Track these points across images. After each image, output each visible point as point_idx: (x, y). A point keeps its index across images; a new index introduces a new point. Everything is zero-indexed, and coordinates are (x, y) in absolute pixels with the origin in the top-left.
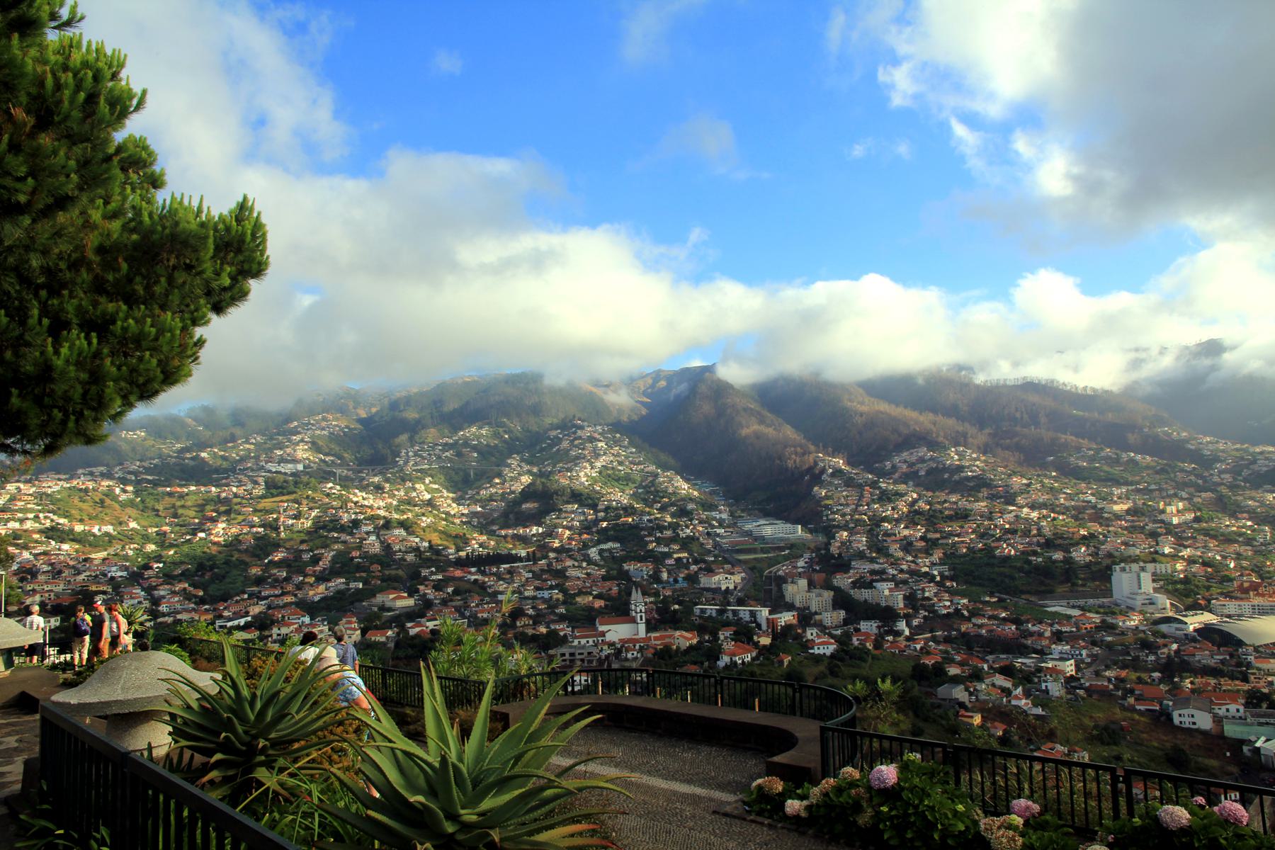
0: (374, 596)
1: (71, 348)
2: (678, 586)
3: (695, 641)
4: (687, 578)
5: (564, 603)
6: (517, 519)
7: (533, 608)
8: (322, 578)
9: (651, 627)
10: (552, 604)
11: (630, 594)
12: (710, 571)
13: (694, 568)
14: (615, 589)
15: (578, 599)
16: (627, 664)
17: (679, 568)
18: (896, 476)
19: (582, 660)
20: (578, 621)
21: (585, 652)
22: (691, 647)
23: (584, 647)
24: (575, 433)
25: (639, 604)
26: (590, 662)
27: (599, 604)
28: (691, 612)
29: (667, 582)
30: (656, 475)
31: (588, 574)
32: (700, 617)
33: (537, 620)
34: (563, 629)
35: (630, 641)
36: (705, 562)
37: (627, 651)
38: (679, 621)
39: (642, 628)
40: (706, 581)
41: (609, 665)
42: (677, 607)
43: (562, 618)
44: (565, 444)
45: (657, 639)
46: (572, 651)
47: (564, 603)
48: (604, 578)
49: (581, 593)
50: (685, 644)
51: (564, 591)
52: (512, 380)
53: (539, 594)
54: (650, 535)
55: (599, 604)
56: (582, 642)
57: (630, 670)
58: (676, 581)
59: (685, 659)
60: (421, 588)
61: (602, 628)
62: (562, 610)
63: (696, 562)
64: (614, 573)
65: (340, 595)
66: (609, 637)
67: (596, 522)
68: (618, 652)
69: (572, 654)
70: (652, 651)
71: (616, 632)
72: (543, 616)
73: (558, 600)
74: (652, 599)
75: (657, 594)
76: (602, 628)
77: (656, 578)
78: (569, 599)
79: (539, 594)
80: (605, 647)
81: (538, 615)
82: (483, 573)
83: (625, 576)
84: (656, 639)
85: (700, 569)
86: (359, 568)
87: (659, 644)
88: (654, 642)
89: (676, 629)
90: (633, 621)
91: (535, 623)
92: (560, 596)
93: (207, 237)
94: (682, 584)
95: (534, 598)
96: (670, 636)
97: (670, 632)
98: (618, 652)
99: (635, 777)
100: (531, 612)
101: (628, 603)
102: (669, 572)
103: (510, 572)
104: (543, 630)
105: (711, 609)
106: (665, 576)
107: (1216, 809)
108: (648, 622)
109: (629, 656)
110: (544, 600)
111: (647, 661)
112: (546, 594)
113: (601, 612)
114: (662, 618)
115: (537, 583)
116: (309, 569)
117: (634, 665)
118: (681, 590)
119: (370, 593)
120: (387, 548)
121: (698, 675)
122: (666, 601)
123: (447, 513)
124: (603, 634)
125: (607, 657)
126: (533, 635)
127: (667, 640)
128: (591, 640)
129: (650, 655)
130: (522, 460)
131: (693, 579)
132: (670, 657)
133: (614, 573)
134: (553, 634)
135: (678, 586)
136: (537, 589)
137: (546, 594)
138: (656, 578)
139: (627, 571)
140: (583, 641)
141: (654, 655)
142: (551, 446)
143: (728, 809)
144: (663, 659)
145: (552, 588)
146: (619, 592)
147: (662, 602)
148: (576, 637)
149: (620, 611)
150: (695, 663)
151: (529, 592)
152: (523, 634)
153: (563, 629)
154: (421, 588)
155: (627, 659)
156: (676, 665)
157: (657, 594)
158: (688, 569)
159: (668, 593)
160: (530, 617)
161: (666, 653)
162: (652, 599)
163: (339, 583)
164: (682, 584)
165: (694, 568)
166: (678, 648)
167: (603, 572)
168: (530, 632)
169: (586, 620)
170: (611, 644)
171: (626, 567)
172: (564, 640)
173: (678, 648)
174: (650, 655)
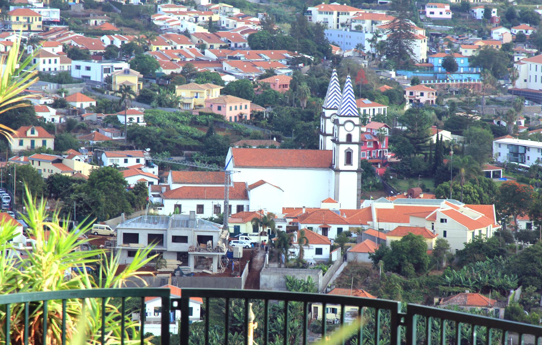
2: (454, 80)
3: (489, 231)
4: (485, 61)
5: (144, 98)
7: (58, 104)
9: (373, 182)
10: (110, 105)
11: (321, 91)
13: (502, 34)
14: (283, 74)
15: (183, 92)
16: (301, 276)
17: (461, 31)
18: (29, 260)
19: (183, 257)
20: (177, 150)
21: (192, 236)
22: (477, 248)
23: (188, 222)
25: (346, 121)
26: (202, 261)
27: (236, 109)
28: (482, 152)
29: (428, 67)
31: (213, 27)
32: (509, 168)
33: (67, 137)
34: (136, 168)
35: (311, 215)
37: (304, 241)
38: (449, 174)
39: (350, 182)
41: (254, 279)
42: (446, 135)
43: (135, 140)
45: (389, 217)
46: (156, 229)
47: (144, 98)
48: (257, 43)
49: (189, 76)
50: (460, 237)
51: (145, 67)
53: (77, 69)
55: (236, 109)
56: (183, 208)
57: (308, 299)
58: (450, 66)
59: (461, 274)
61: (240, 175)
62: (135, 117)
63: (509, 19)
64: (285, 29)
66: (257, 202)
68: (279, 244)
69: (156, 238)
70: (373, 247)
71: (281, 189)
72: (85, 129)
73: (126, 89)
74: (380, 109)
75: (394, 97)
76: (240, 175)
77: (395, 52)
78: (156, 89)
79: (77, 69)
80: (247, 227)
81: (70, 126)
83: (311, 42)
84: (384, 215)
85: (520, 39)
87: (391, 232)
88: (376, 224)
89: (439, 195)
90: (328, 163)
91: (59, 148)
92: (134, 80)
94: (465, 76)
95: (63, 78)
96: (422, 213)
97: (424, 202)
98: (279, 244)
99: (228, 193)
100: (51, 115)
101: (313, 116)
102: (433, 40)
104: (81, 166)
106: (420, 49)
107: (232, 185)
108: (366, 170)
109: (309, 255)
110: (91, 88)
111: (354, 275)
112: (96, 71)
113: (239, 132)
114: (410, 162)
115: (73, 38)
117: (321, 281)
118: (463, 90)
121: (490, 324)
122: (415, 117)
124: (243, 192)
125: (249, 254)
127: (414, 222)
128: (209, 205)
129: (364, 259)
132: (419, 267)
133: (285, 29)
134: (107, 179)
135: (454, 80)
136: (73, 54)
137: (96, 71)
138: (395, 52)
139: (320, 28)
140: (189, 206)
141: (376, 258)
143: (309, 316)
144: (398, 270)
145: (110, 54)
146: (294, 84)
147: (410, 118)
148: (170, 194)
149: (294, 131)
150: (486, 290)
151: (51, 62)
153: (136, 168)
155: (301, 264)
156: (434, 289)
158: (485, 35)
159: (427, 97)
160: (50, 128)
161: (404, 257)
162: (380, 109)
164: (465, 76)
165: (502, 34)
166: (442, 246)
167: (254, 24)
168: (46, 169)
169: (202, 147)
170: (262, 221)
171: (317, 16)
172: (135, 200)
173: (442, 246)
174: (364, 259)
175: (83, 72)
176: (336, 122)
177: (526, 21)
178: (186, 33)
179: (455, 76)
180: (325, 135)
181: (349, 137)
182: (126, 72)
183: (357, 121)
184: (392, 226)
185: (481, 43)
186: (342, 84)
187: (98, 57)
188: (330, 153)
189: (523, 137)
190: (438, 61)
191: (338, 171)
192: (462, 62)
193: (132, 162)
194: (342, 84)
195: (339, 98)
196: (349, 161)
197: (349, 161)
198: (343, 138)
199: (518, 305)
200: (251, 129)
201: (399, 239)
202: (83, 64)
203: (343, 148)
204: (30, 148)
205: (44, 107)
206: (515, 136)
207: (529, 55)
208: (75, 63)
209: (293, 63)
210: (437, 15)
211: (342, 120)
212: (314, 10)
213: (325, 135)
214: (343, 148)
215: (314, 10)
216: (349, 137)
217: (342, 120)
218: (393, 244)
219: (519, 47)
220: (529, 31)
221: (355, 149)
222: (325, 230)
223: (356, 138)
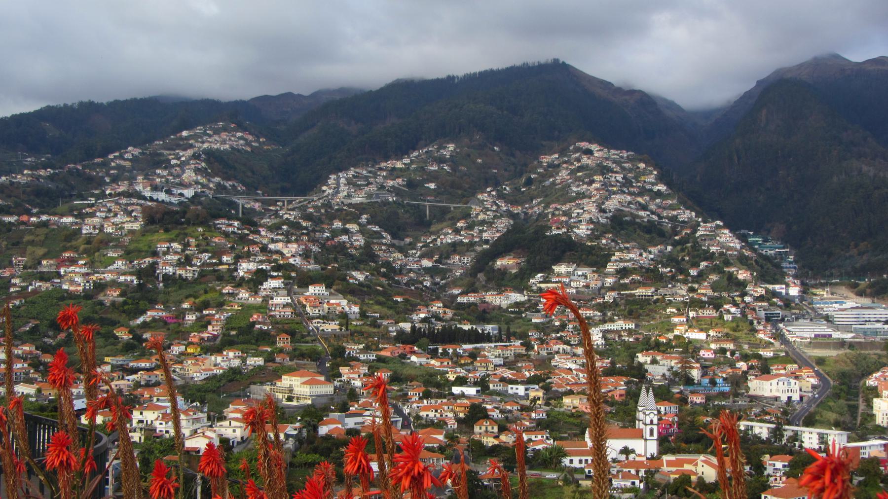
0: (279, 378)
1: (568, 274)
6: (489, 280)
8: (213, 347)
9: (665, 445)
12: (764, 369)
13: (742, 365)
15: (567, 401)
17: (719, 364)
24: (578, 160)
25: (649, 411)
30: (695, 227)
36: (759, 357)
40: (759, 387)
44: (564, 174)
52: (775, 72)
54: (680, 314)
58: (713, 383)
60: (344, 370)
63: (745, 357)
65: (233, 374)
67: (602, 290)
72: (515, 420)
82: (434, 354)
86: (265, 338)
93: (39, 457)
102: (704, 369)
103: (473, 355)
105: (762, 430)
114: (682, 437)
116: (194, 337)
119: (269, 374)
120: (299, 310)
123: (387, 264)
126: (495, 447)
127: (687, 467)
130: (501, 196)
131: (738, 382)
139: (641, 365)
142: (544, 177)
152: (479, 444)
154: (344, 370)
157: (683, 401)
158: (732, 365)
159: (698, 399)
160: (495, 421)
163: (230, 359)
175: (514, 391)
176: (644, 413)
177: (755, 358)
178: (570, 369)
179: (716, 388)
180: (639, 420)
181: (652, 421)
182: (537, 390)
183: (656, 412)
184: (674, 469)
185: (730, 370)
186: (648, 391)
187: (522, 383)
188: (642, 430)
189: (752, 420)
190: (706, 381)
191: (646, 440)
192: (719, 381)
193: (539, 437)
194: (648, 391)
195: (646, 400)
196: (652, 434)
197: (652, 434)
198: (648, 422)
199: (422, 465)
200: (114, 316)
201: (677, 476)
202: (514, 387)
203: (649, 427)
204: (806, 489)
205: (492, 410)
206: (748, 420)
207: (756, 376)
208: (510, 386)
209: (626, 383)
210: (706, 356)
211: (647, 412)
212: (639, 355)
213: (639, 420)
214: (649, 427)
215: (639, 355)
216: (652, 421)
217: (647, 412)
218: (675, 479)
219: (751, 372)
220: (754, 362)
221: (655, 428)
222: (637, 472)
223: (655, 421)
